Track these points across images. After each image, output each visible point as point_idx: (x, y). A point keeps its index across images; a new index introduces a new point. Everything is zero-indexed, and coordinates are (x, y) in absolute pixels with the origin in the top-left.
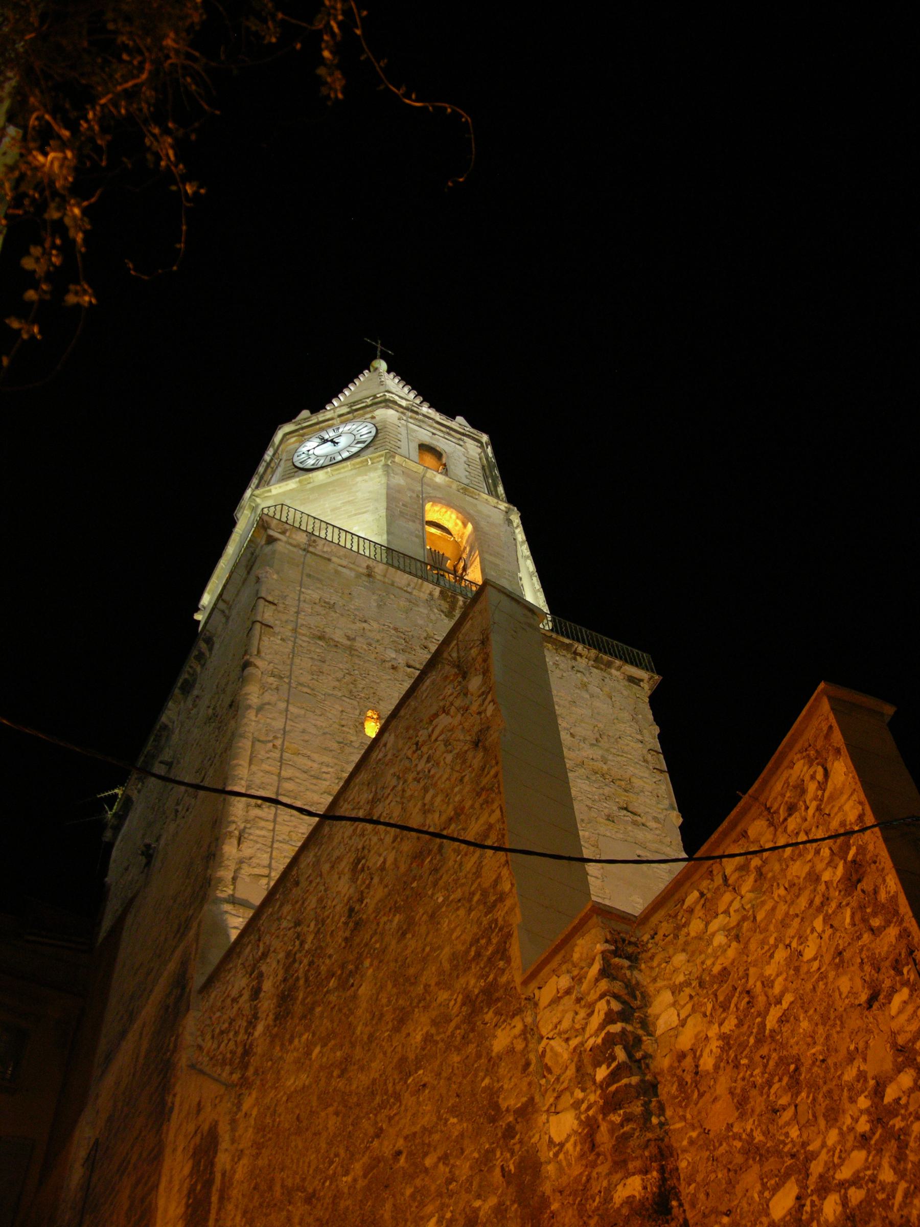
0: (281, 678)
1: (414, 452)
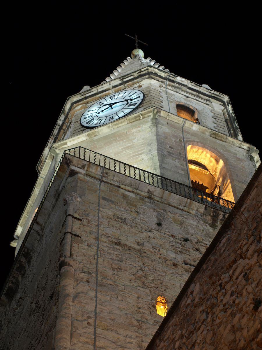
0: (89, 273)
1: (174, 110)
